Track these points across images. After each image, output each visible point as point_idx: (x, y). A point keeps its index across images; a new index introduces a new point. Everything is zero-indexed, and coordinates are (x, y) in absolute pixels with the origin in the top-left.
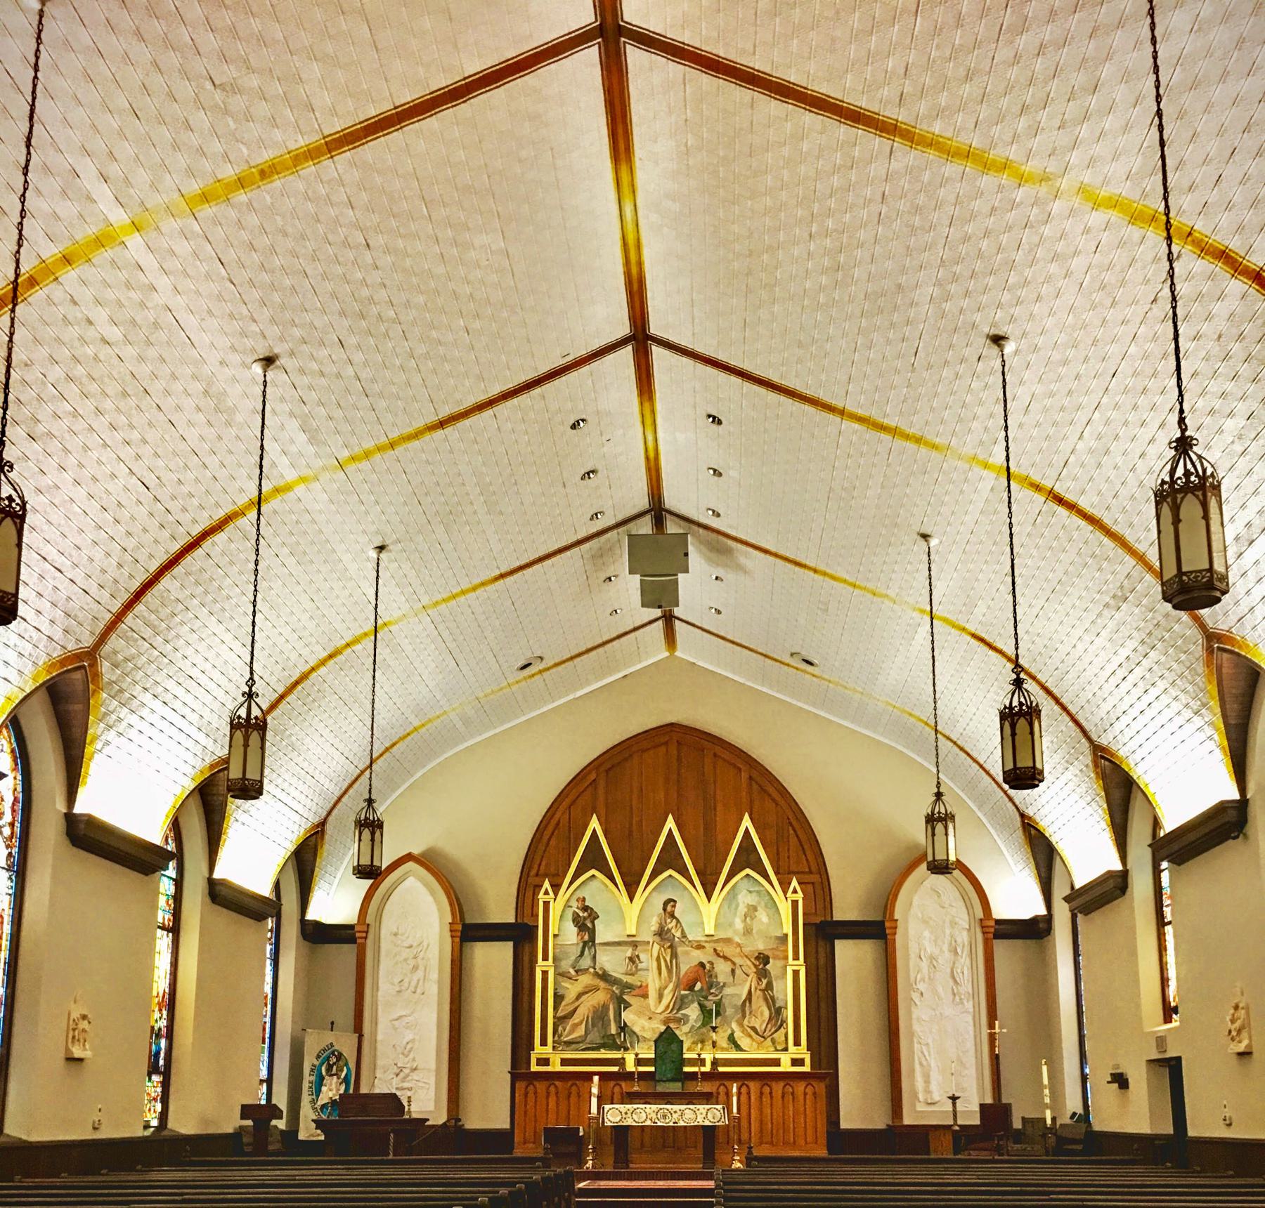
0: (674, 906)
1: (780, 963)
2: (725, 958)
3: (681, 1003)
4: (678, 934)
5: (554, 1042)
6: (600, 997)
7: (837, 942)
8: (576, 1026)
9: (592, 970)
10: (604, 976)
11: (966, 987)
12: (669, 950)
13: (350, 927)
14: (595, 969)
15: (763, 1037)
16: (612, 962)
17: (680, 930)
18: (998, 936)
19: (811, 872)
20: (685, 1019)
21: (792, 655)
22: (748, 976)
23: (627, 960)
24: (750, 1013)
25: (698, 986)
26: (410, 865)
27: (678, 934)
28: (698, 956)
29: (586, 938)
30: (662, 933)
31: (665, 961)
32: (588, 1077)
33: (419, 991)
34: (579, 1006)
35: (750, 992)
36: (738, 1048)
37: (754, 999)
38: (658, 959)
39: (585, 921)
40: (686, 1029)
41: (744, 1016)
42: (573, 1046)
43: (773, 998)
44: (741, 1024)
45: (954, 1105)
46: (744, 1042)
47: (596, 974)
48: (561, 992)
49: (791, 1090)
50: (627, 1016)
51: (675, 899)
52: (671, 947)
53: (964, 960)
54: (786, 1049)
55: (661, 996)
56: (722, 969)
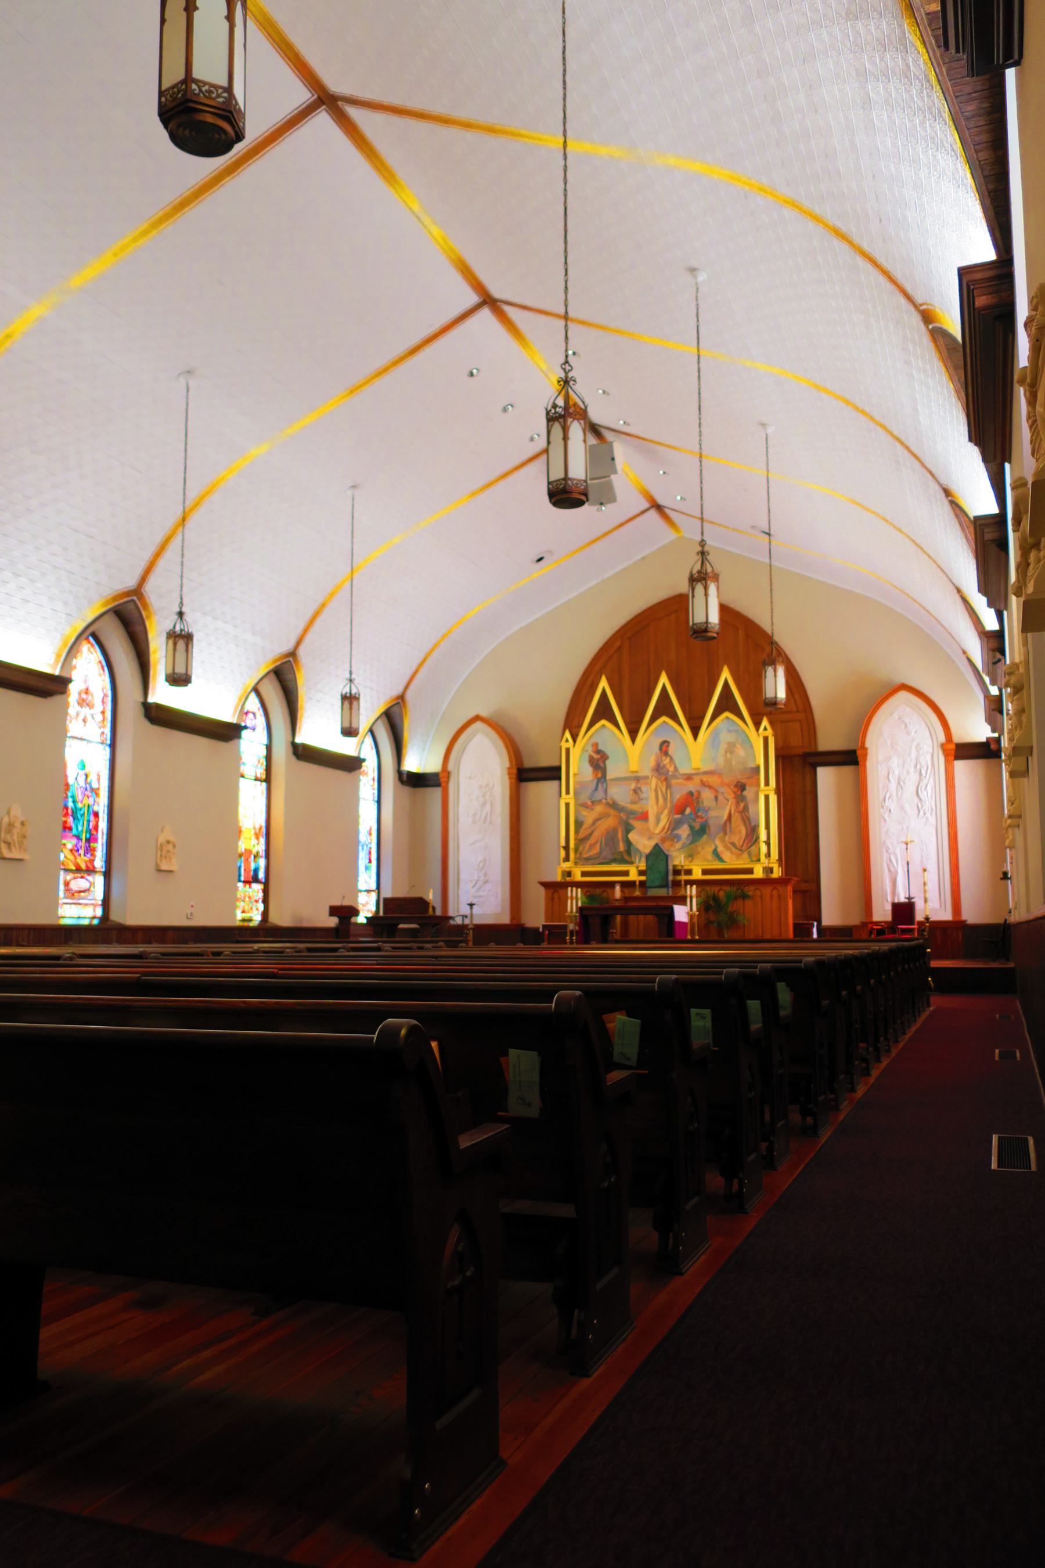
0: (668, 746)
1: (754, 789)
2: (710, 787)
3: (675, 825)
4: (671, 769)
5: (576, 858)
6: (609, 823)
7: (821, 771)
8: (592, 846)
9: (604, 801)
10: (614, 805)
11: (929, 803)
12: (665, 783)
13: (436, 775)
14: (606, 800)
15: (740, 850)
16: (619, 793)
17: (673, 766)
18: (958, 757)
19: (798, 711)
20: (678, 838)
21: (753, 527)
22: (728, 800)
23: (632, 792)
24: (731, 831)
25: (688, 811)
26: (478, 725)
27: (671, 769)
28: (691, 787)
29: (600, 775)
30: (658, 769)
31: (662, 792)
32: (612, 885)
33: (488, 820)
34: (596, 828)
35: (730, 815)
36: (721, 860)
37: (733, 820)
38: (656, 790)
39: (598, 761)
40: (678, 845)
41: (725, 833)
42: (591, 861)
43: (748, 818)
44: (723, 841)
45: (471, 908)
46: (726, 855)
47: (607, 804)
48: (581, 819)
49: (759, 893)
50: (632, 836)
51: (665, 739)
52: (666, 779)
53: (929, 781)
54: (759, 860)
55: (658, 820)
56: (707, 796)
